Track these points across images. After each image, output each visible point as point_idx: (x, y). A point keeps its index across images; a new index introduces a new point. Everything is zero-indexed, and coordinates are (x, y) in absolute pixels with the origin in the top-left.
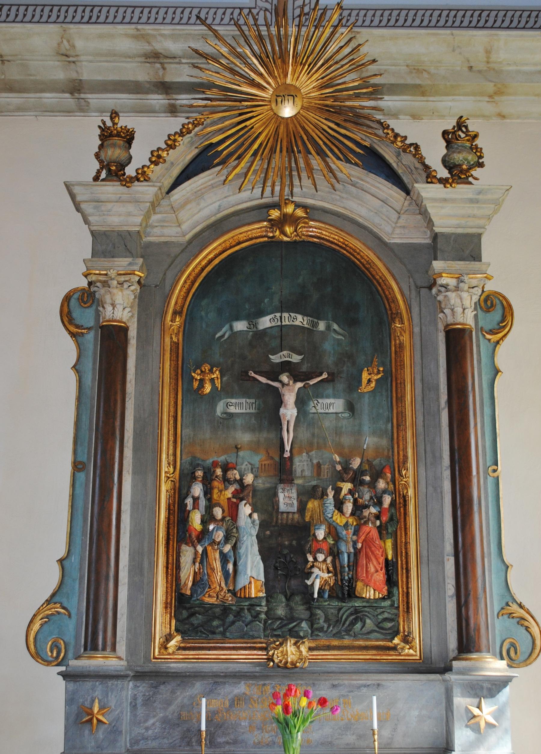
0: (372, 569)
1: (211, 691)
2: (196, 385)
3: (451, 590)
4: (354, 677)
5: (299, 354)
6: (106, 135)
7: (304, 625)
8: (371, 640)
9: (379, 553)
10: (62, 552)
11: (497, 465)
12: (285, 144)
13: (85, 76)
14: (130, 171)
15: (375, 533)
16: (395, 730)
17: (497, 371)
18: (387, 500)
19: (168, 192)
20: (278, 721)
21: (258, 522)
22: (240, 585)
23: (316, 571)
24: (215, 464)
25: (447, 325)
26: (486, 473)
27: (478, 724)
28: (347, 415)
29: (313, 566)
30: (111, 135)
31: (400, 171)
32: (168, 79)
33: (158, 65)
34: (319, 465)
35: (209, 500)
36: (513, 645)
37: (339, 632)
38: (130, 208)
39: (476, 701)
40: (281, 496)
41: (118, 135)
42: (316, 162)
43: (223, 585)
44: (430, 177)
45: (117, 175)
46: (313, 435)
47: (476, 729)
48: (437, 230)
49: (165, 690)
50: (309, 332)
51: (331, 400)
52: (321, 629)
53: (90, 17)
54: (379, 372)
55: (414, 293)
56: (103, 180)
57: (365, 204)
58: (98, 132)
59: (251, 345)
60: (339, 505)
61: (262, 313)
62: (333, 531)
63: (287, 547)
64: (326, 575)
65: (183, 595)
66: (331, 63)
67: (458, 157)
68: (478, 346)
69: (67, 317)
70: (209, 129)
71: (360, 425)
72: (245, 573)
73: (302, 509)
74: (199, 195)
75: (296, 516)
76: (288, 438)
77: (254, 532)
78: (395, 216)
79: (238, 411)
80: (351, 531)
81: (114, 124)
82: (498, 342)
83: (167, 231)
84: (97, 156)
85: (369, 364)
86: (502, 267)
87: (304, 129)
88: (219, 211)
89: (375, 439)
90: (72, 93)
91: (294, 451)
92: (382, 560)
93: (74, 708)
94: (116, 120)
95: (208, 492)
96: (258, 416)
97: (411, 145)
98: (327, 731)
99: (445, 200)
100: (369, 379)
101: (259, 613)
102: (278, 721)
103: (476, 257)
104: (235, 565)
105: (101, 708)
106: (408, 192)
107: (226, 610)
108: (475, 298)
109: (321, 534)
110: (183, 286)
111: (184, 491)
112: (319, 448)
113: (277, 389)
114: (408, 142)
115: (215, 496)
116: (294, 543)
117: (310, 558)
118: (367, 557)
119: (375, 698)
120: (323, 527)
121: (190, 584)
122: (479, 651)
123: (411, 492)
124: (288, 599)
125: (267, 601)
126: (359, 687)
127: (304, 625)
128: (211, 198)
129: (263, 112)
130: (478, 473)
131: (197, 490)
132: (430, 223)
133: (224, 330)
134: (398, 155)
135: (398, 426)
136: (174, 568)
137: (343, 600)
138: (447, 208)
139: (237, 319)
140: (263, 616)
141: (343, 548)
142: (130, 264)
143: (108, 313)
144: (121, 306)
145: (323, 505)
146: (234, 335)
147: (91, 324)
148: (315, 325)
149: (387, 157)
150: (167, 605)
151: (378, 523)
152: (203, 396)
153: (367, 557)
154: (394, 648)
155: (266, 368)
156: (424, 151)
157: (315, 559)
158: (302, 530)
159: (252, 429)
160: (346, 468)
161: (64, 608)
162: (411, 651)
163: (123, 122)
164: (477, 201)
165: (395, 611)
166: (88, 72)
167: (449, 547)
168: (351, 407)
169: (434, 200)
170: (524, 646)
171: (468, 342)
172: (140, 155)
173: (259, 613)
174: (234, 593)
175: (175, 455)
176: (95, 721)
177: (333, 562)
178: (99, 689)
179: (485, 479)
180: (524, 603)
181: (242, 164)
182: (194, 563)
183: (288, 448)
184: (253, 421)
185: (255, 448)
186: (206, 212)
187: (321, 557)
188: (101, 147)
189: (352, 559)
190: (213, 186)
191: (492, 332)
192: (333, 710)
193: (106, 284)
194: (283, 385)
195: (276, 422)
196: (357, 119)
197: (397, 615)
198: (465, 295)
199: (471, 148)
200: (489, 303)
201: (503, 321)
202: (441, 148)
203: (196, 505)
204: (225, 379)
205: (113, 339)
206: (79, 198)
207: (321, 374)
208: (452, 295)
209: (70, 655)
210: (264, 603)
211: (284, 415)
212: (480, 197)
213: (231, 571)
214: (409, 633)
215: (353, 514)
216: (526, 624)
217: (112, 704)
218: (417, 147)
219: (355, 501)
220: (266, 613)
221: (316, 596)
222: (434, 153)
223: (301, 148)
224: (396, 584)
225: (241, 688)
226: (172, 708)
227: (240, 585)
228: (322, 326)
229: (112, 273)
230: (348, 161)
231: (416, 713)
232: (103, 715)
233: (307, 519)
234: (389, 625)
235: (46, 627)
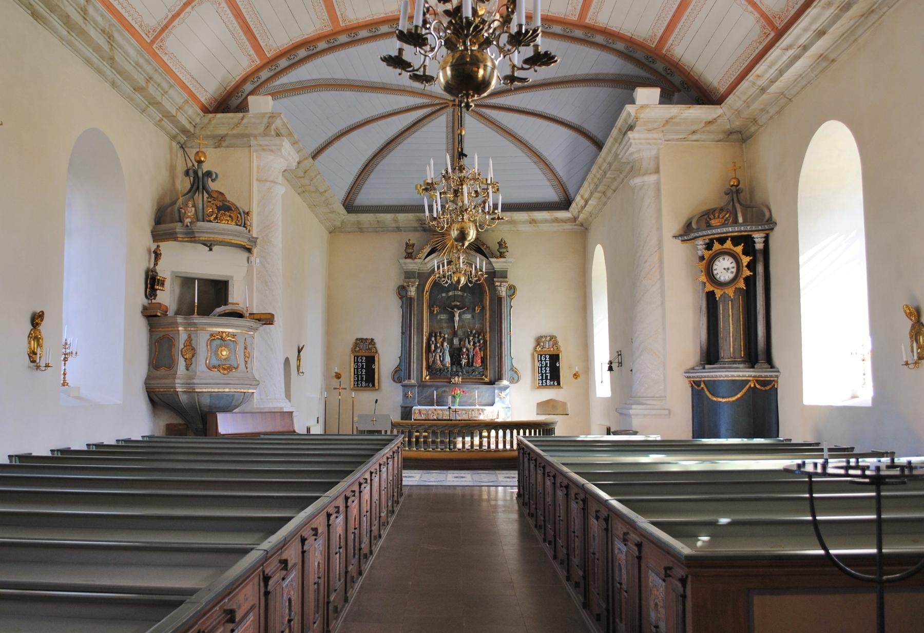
50: (462, 296)
62: (467, 350)
63: (456, 360)
76: (456, 325)
86: (512, 279)
100: (478, 310)
131: (433, 339)
138: (498, 264)
144: (412, 292)
158: (460, 349)
168: (473, 317)
185: (448, 327)
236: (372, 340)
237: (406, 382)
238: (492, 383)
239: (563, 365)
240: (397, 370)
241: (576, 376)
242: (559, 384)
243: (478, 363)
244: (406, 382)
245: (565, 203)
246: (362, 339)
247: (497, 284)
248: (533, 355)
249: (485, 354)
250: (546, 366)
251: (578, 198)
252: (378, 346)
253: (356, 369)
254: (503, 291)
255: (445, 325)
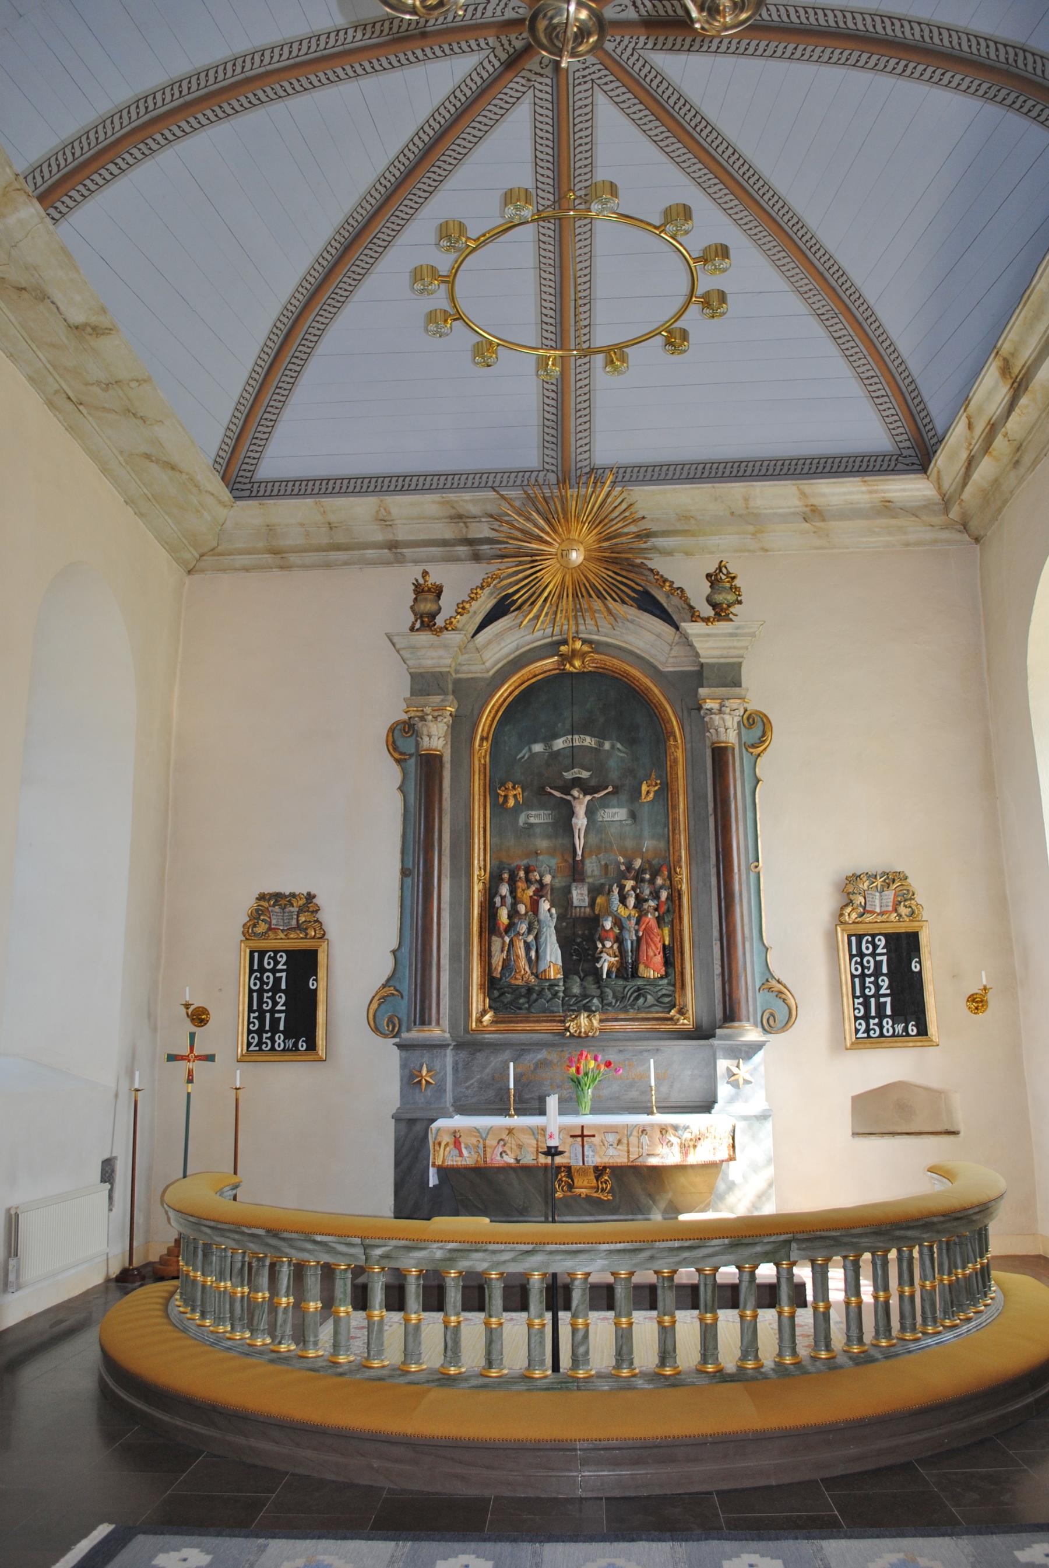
0: (651, 954)
1: (519, 1056)
2: (501, 800)
3: (718, 970)
4: (637, 1043)
5: (588, 770)
6: (419, 590)
7: (595, 1001)
8: (651, 1012)
9: (657, 940)
10: (394, 945)
11: (758, 861)
12: (570, 591)
13: (400, 538)
14: (440, 621)
15: (653, 923)
16: (671, 1086)
17: (758, 781)
18: (664, 895)
19: (473, 637)
20: (572, 1080)
21: (555, 916)
22: (541, 969)
23: (604, 955)
24: (518, 868)
25: (713, 743)
26: (748, 869)
27: (737, 1080)
28: (629, 822)
29: (601, 952)
30: (423, 591)
31: (670, 610)
32: (469, 536)
33: (462, 525)
34: (606, 866)
35: (514, 898)
36: (772, 1015)
37: (625, 1007)
38: (441, 652)
39: (735, 1062)
40: (574, 893)
41: (429, 590)
42: (597, 604)
43: (527, 969)
44: (694, 616)
45: (428, 626)
46: (601, 840)
47: (736, 1085)
48: (702, 660)
49: (480, 1057)
50: (596, 751)
51: (617, 810)
52: (610, 1004)
53: (403, 486)
54: (656, 784)
55: (686, 714)
56: (418, 630)
57: (642, 637)
58: (413, 587)
59: (548, 765)
60: (623, 900)
61: (556, 736)
62: (618, 922)
63: (580, 939)
64: (613, 959)
65: (494, 978)
66: (606, 521)
67: (719, 598)
68: (741, 759)
69: (393, 746)
70: (505, 582)
71: (641, 830)
72: (545, 958)
73: (592, 904)
74: (499, 636)
75: (588, 910)
77: (553, 924)
78: (667, 648)
79: (537, 821)
80: (633, 922)
81: (426, 581)
82: (759, 755)
83: (474, 668)
84: (412, 607)
85: (648, 777)
86: (758, 690)
87: (586, 577)
88: (517, 649)
89: (655, 842)
90: (390, 549)
91: (586, 855)
92: (660, 945)
93: (407, 1071)
94: (427, 578)
95: (513, 891)
96: (554, 825)
97: (678, 588)
98: (615, 1088)
99: (708, 635)
100: (648, 791)
101: (557, 992)
102: (572, 1080)
103: (737, 684)
104: (537, 951)
105: (428, 1071)
106: (677, 628)
107: (530, 990)
108: (737, 719)
109: (608, 924)
110: (488, 716)
111: (493, 891)
112: (606, 851)
113: (569, 802)
114: (675, 586)
115: (519, 895)
116: (586, 932)
117: (600, 946)
118: (647, 943)
119: (652, 1061)
120: (610, 919)
121: (500, 969)
122: (740, 1020)
123: (684, 887)
124: (582, 980)
125: (564, 982)
126: (641, 1052)
127: (595, 1001)
128: (506, 640)
129: (552, 564)
130: (739, 870)
131: (504, 889)
132: (697, 655)
133: (524, 752)
134: (668, 597)
135: (674, 830)
136: (486, 956)
137: (626, 979)
139: (535, 742)
140: (561, 994)
141: (627, 936)
142: (443, 700)
143: (425, 742)
144: (436, 737)
145: (609, 902)
146: (533, 756)
147: (413, 751)
148: (601, 745)
149: (659, 598)
150: (482, 986)
151: (657, 914)
152: (507, 809)
153: (647, 943)
154: (671, 1019)
155: (560, 783)
156: (689, 593)
157: (604, 946)
158: (593, 922)
159: (549, 837)
160: (629, 868)
161: (397, 990)
162: (685, 1021)
163: (432, 580)
164: (736, 635)
165: (672, 988)
166: (402, 534)
167: (716, 934)
168: (633, 815)
169: (699, 635)
170: (781, 1014)
171: (730, 758)
172: (448, 603)
173: (557, 992)
174: (537, 976)
175: (485, 860)
176: (424, 1081)
177: (619, 948)
178: (426, 1056)
179: (748, 874)
180: (782, 979)
181: (535, 610)
182: (502, 951)
183: (579, 852)
184: (550, 829)
185: (552, 852)
186: (506, 650)
187: (608, 944)
188: (415, 600)
189: (635, 944)
190: (510, 628)
191: (753, 746)
192: (616, 1071)
193: (422, 719)
194: (575, 798)
195: (569, 830)
196: (633, 567)
197: (674, 992)
198: (727, 717)
199: (731, 588)
200: (751, 721)
201: (763, 736)
202: (706, 588)
203: (503, 904)
204: (526, 794)
205: (429, 767)
206: (398, 646)
207: (606, 788)
208: (716, 718)
209: (404, 1028)
210: (561, 984)
211: (576, 824)
212: (738, 631)
213: (533, 957)
214: (685, 1006)
215: (635, 907)
216: (783, 996)
217: (437, 1068)
218: (682, 590)
219: (637, 897)
220: (564, 992)
221: (605, 976)
222: (698, 592)
223: (584, 593)
224: (673, 965)
225: (543, 1055)
226: (487, 1070)
227: (541, 969)
228: (607, 745)
229: (428, 710)
230: (623, 602)
231: (689, 1073)
232: (431, 1077)
233: (597, 912)
234: (667, 1000)
235: (383, 1006)
236: (310, 897)
237: (415, 1035)
238: (702, 1033)
239: (932, 967)
240: (388, 993)
241: (977, 1002)
242: (923, 1031)
243: (652, 969)
244: (415, 1035)
245: (918, 453)
246: (277, 896)
247: (709, 704)
248: (832, 937)
249: (676, 935)
250: (877, 973)
251: (958, 431)
252: (330, 917)
253: (256, 995)
254: (727, 729)
255: (543, 844)
